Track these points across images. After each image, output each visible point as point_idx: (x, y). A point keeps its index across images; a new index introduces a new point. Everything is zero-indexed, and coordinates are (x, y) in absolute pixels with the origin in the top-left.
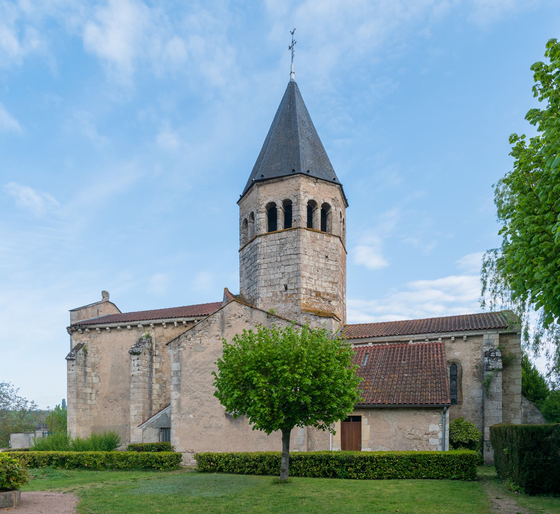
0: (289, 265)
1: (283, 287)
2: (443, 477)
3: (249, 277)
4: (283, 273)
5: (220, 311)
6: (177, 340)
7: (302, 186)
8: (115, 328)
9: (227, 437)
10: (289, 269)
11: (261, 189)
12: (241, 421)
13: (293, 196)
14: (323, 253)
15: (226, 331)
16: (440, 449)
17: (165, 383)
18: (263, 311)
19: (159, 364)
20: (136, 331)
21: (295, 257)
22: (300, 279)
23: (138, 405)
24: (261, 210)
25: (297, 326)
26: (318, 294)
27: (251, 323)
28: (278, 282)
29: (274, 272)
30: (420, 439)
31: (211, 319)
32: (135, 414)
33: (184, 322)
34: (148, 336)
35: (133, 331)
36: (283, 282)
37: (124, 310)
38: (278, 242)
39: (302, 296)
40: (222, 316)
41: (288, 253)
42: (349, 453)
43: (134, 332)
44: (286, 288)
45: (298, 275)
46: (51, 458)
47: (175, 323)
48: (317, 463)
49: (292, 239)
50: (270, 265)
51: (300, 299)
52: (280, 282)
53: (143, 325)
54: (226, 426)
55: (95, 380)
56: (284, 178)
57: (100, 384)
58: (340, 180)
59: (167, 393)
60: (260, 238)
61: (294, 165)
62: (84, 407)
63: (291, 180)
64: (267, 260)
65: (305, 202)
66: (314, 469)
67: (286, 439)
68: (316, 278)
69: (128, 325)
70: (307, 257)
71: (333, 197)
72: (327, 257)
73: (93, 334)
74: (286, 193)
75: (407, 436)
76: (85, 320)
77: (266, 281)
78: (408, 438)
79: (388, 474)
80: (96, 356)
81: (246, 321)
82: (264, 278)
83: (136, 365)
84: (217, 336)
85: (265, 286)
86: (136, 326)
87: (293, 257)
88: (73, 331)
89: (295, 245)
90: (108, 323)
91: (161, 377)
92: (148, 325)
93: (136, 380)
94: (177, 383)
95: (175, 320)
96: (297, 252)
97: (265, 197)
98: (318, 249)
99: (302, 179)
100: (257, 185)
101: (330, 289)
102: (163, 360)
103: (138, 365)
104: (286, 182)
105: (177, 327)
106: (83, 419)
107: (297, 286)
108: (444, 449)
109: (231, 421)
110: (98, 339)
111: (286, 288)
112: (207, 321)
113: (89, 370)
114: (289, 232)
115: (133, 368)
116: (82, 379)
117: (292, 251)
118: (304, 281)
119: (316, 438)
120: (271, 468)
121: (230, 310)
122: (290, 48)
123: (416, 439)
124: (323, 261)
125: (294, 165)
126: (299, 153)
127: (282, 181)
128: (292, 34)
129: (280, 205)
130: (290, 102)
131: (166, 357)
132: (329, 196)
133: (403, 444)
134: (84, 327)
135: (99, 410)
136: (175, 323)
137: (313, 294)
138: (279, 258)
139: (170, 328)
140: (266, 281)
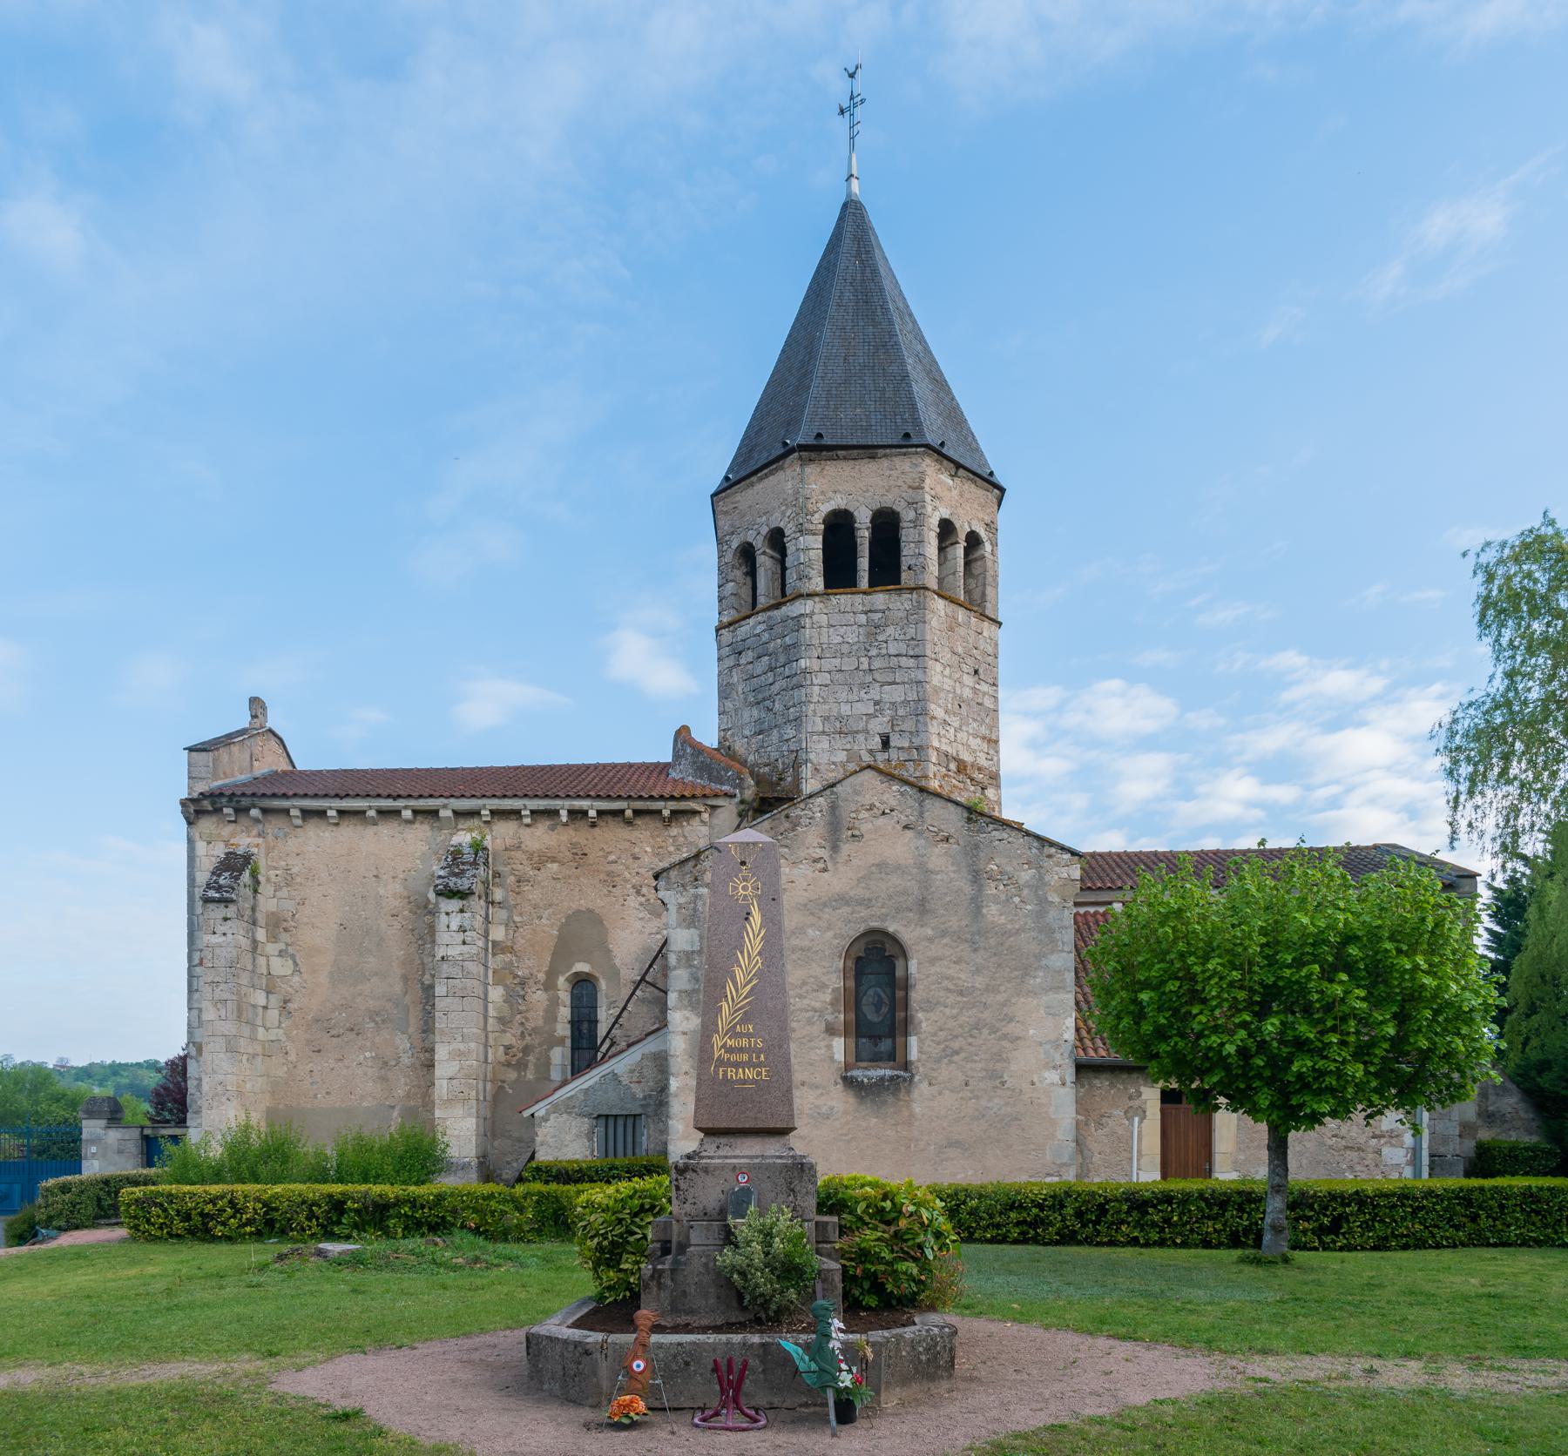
0: (894, 683)
1: (878, 739)
2: (1539, 1243)
3: (761, 700)
4: (876, 703)
5: (828, 792)
6: (691, 864)
7: (928, 481)
8: (359, 814)
9: (849, 1142)
10: (895, 694)
11: (811, 470)
12: (891, 1099)
13: (903, 503)
14: (969, 661)
15: (846, 848)
16: (1408, 1172)
17: (523, 984)
18: (957, 803)
19: (502, 928)
20: (426, 827)
21: (912, 662)
22: (926, 724)
23: (462, 1046)
24: (812, 527)
25: (1053, 850)
26: (962, 767)
27: (920, 833)
28: (861, 725)
29: (851, 698)
30: (1359, 1149)
31: (798, 812)
32: (450, 1074)
33: (592, 813)
34: (478, 847)
35: (417, 825)
36: (879, 725)
37: (307, 760)
38: (862, 619)
39: (932, 769)
40: (833, 808)
41: (892, 651)
42: (1177, 1185)
43: (422, 830)
44: (886, 743)
45: (920, 711)
46: (338, 1205)
47: (564, 813)
48: (1216, 1210)
49: (902, 614)
50: (839, 676)
51: (926, 777)
52: (870, 726)
53: (455, 812)
54: (846, 1112)
55: (280, 967)
56: (881, 452)
57: (296, 979)
58: (1000, 478)
59: (529, 1015)
60: (810, 603)
61: (905, 421)
62: (251, 1051)
63: (897, 461)
64: (829, 664)
65: (934, 522)
66: (1209, 1227)
67: (1278, 1148)
68: (956, 724)
69: (406, 807)
70: (938, 667)
71: (987, 519)
72: (976, 672)
73: (274, 826)
74: (883, 491)
75: (1330, 1142)
76: (227, 781)
77: (826, 719)
78: (1331, 1147)
79: (1403, 1236)
80: (284, 893)
81: (906, 827)
82: (823, 710)
83: (454, 927)
84: (816, 861)
85: (823, 732)
86: (433, 813)
87: (904, 661)
88: (200, 813)
89: (911, 632)
90: (337, 796)
91: (508, 967)
92: (475, 814)
93: (456, 972)
94: (688, 987)
95: (563, 806)
96: (917, 651)
97: (823, 493)
98: (960, 650)
99: (928, 461)
100: (800, 458)
101: (983, 756)
102: (517, 919)
103: (462, 929)
104: (885, 463)
105: (565, 825)
106: (248, 1086)
107: (917, 742)
108: (1417, 1174)
109: (861, 1099)
110: (292, 844)
111: (886, 743)
112: (787, 817)
113: (261, 935)
114: (894, 597)
115: (443, 937)
116: (246, 960)
117: (903, 648)
118: (934, 728)
119: (1095, 1147)
120: (1084, 1226)
121: (857, 793)
122: (842, 112)
123: (1351, 1148)
124: (969, 680)
125: (905, 421)
126: (910, 392)
127: (873, 457)
128: (852, 76)
129: (863, 518)
130: (859, 254)
131: (528, 908)
132: (981, 515)
133: (1318, 1163)
134: (245, 802)
135: (292, 1057)
136: (564, 813)
137: (953, 766)
138: (864, 660)
139: (542, 827)
140: (826, 719)
